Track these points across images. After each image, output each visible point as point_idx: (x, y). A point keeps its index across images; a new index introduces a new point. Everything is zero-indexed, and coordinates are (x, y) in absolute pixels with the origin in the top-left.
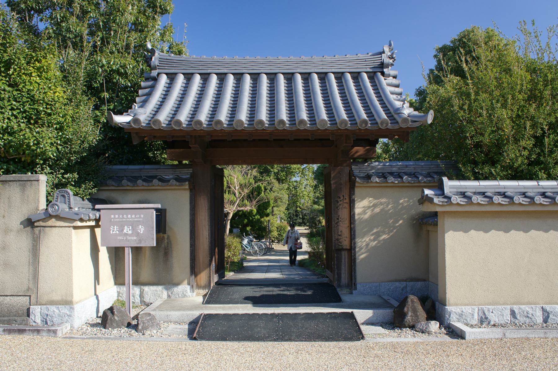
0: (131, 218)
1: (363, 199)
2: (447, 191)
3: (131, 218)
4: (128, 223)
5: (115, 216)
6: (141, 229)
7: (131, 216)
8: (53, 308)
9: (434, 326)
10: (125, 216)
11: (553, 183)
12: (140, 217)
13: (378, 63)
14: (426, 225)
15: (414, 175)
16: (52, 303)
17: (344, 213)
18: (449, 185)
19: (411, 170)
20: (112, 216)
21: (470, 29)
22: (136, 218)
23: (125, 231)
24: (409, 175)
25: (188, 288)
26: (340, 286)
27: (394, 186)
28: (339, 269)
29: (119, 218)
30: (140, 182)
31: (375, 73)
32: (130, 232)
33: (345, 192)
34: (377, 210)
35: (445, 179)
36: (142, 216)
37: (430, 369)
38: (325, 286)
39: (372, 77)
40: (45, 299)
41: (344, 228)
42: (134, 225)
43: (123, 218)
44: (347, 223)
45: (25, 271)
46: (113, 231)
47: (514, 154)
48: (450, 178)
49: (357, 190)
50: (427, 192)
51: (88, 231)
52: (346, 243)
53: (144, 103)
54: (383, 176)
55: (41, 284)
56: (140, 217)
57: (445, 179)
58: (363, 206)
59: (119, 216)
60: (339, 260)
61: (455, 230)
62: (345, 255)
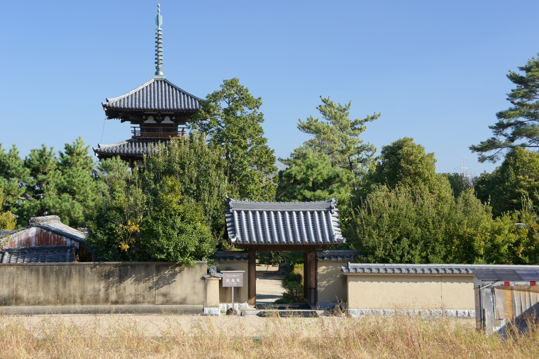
1: (322, 266)
2: (349, 267)
4: (233, 278)
6: (238, 280)
7: (234, 275)
8: (212, 308)
9: (344, 314)
13: (328, 207)
14: (344, 280)
15: (342, 257)
16: (212, 307)
17: (313, 273)
18: (351, 265)
19: (341, 254)
21: (410, 137)
24: (341, 257)
25: (247, 304)
26: (311, 304)
27: (334, 262)
28: (310, 297)
30: (228, 259)
31: (328, 211)
33: (314, 264)
34: (329, 270)
35: (349, 263)
38: (302, 298)
39: (326, 213)
40: (209, 305)
41: (312, 279)
42: (235, 279)
44: (314, 277)
45: (202, 295)
47: (380, 253)
48: (351, 262)
49: (318, 264)
50: (342, 267)
52: (313, 286)
53: (234, 232)
54: (329, 257)
55: (207, 300)
57: (349, 263)
58: (322, 269)
60: (311, 293)
62: (313, 291)
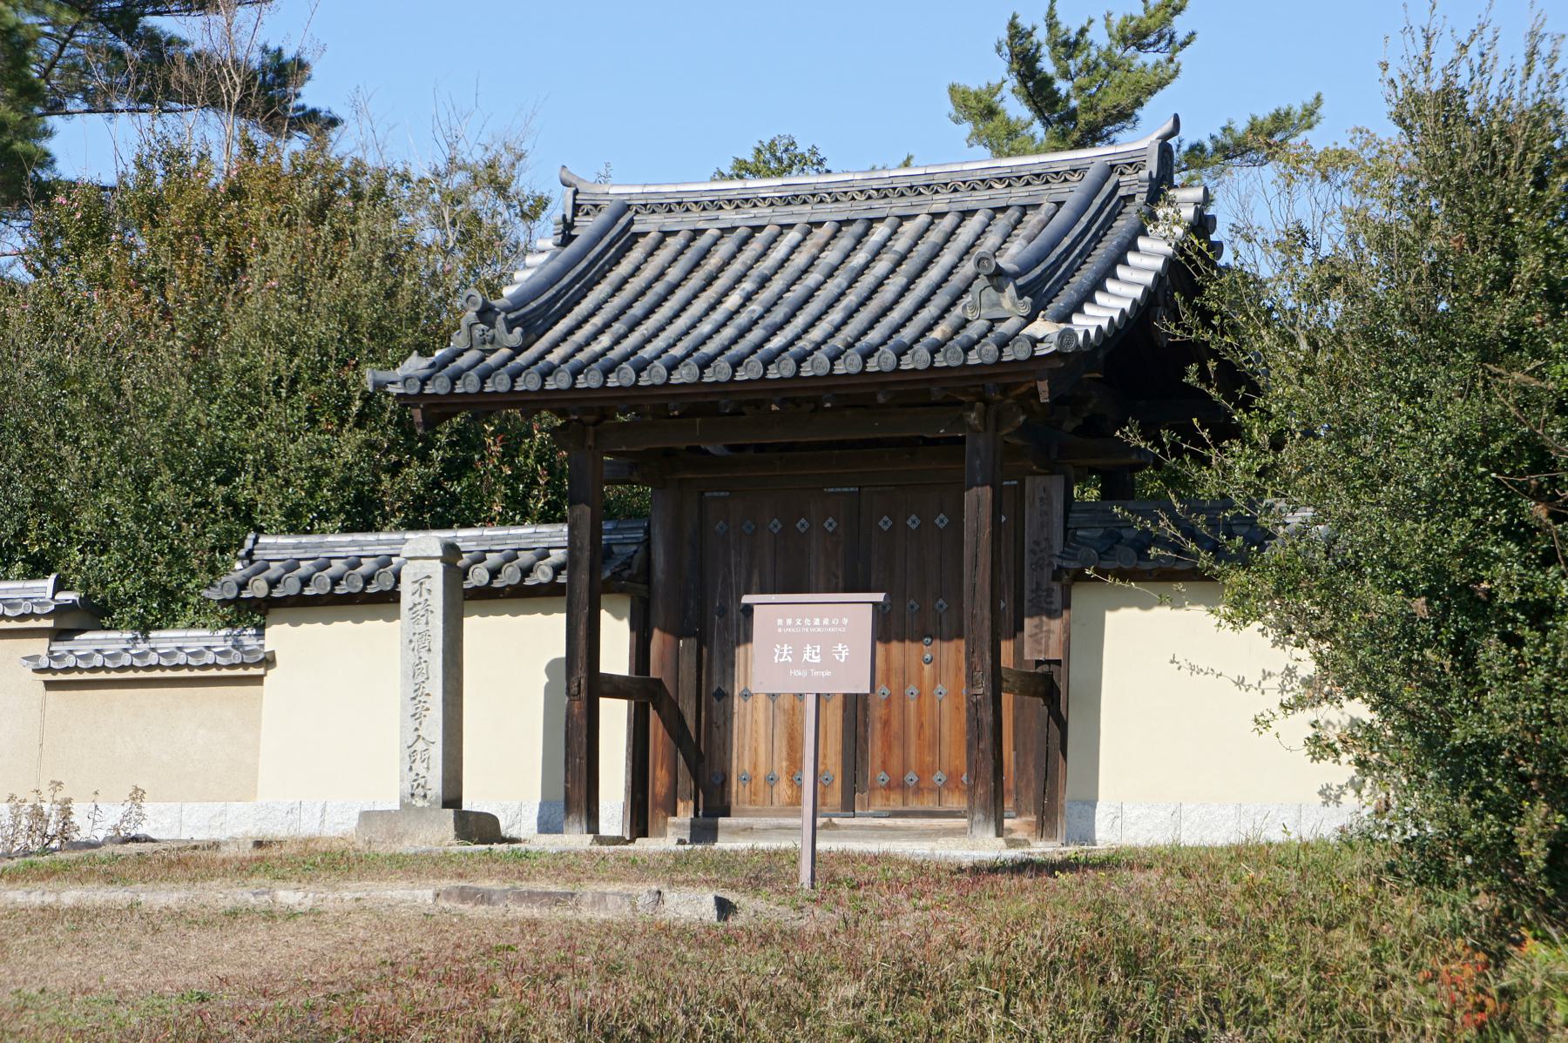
0: (821, 625)
3: (821, 625)
4: (814, 639)
5: (794, 622)
10: (826, 622)
11: (12, 18)
12: (841, 625)
20: (780, 622)
22: (831, 625)
23: (806, 657)
29: (794, 625)
32: (817, 659)
36: (845, 621)
37: (251, 1035)
42: (827, 642)
43: (812, 626)
46: (781, 656)
51: (475, 627)
56: (841, 625)
59: (794, 622)
61: (1114, 608)
